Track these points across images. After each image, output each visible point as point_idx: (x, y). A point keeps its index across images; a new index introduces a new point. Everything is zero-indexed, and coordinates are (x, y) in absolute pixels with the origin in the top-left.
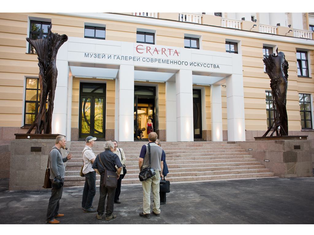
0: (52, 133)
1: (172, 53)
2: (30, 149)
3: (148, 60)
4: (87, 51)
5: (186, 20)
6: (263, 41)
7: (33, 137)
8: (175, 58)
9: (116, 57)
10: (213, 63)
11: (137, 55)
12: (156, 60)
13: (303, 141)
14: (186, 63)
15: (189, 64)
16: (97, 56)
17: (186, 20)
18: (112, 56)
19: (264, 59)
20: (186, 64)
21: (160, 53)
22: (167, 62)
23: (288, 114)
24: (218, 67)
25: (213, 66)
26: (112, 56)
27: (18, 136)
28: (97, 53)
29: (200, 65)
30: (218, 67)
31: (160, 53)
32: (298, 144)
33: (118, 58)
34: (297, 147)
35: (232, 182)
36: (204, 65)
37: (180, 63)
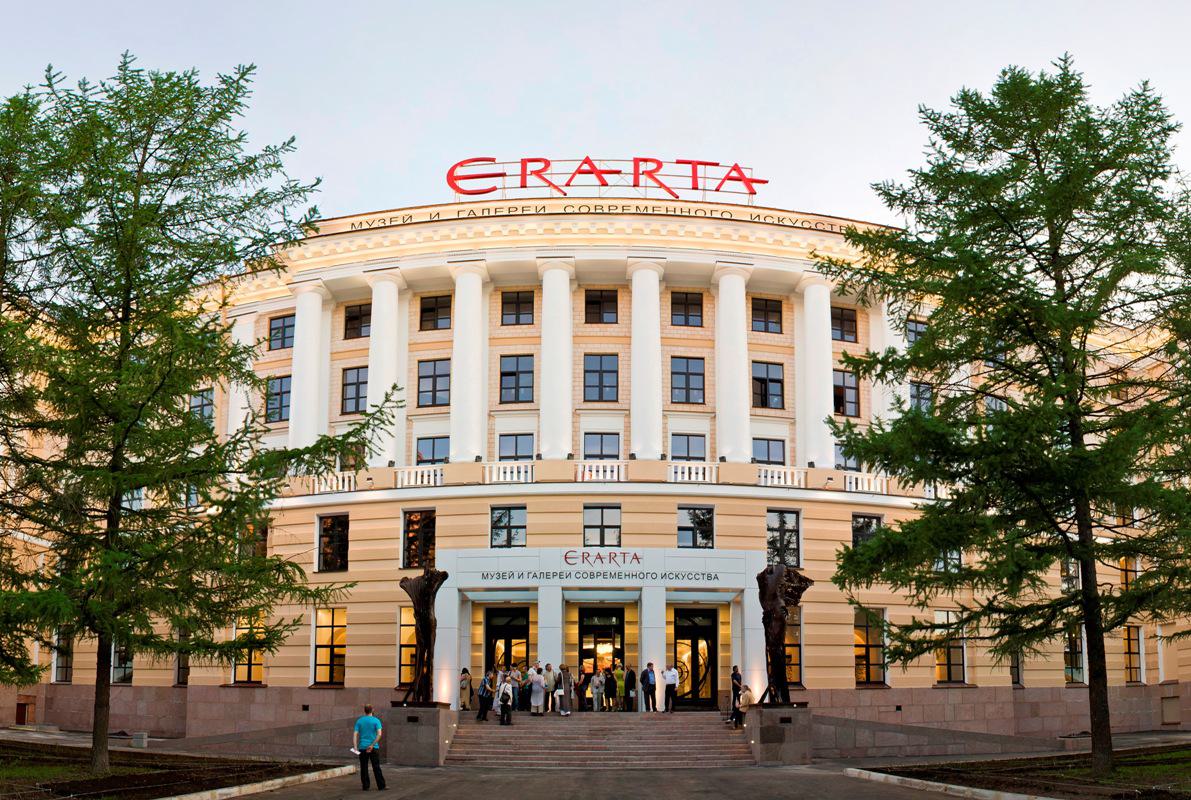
0: (434, 700)
1: (629, 559)
2: (406, 720)
3: (585, 575)
4: (486, 570)
5: (857, 488)
6: (677, 498)
7: (409, 705)
8: (634, 567)
9: (531, 575)
10: (707, 571)
11: (567, 568)
12: (599, 574)
13: (799, 709)
14: (654, 575)
15: (659, 577)
16: (501, 576)
17: (857, 488)
18: (526, 574)
19: (842, 549)
20: (654, 576)
21: (606, 561)
22: (619, 576)
23: (1108, 677)
24: (716, 577)
25: (706, 577)
26: (526, 574)
27: (395, 704)
28: (501, 571)
29: (680, 576)
30: (716, 577)
31: (606, 561)
32: (787, 716)
33: (535, 576)
34: (786, 720)
35: (961, 778)
36: (688, 576)
37: (644, 576)
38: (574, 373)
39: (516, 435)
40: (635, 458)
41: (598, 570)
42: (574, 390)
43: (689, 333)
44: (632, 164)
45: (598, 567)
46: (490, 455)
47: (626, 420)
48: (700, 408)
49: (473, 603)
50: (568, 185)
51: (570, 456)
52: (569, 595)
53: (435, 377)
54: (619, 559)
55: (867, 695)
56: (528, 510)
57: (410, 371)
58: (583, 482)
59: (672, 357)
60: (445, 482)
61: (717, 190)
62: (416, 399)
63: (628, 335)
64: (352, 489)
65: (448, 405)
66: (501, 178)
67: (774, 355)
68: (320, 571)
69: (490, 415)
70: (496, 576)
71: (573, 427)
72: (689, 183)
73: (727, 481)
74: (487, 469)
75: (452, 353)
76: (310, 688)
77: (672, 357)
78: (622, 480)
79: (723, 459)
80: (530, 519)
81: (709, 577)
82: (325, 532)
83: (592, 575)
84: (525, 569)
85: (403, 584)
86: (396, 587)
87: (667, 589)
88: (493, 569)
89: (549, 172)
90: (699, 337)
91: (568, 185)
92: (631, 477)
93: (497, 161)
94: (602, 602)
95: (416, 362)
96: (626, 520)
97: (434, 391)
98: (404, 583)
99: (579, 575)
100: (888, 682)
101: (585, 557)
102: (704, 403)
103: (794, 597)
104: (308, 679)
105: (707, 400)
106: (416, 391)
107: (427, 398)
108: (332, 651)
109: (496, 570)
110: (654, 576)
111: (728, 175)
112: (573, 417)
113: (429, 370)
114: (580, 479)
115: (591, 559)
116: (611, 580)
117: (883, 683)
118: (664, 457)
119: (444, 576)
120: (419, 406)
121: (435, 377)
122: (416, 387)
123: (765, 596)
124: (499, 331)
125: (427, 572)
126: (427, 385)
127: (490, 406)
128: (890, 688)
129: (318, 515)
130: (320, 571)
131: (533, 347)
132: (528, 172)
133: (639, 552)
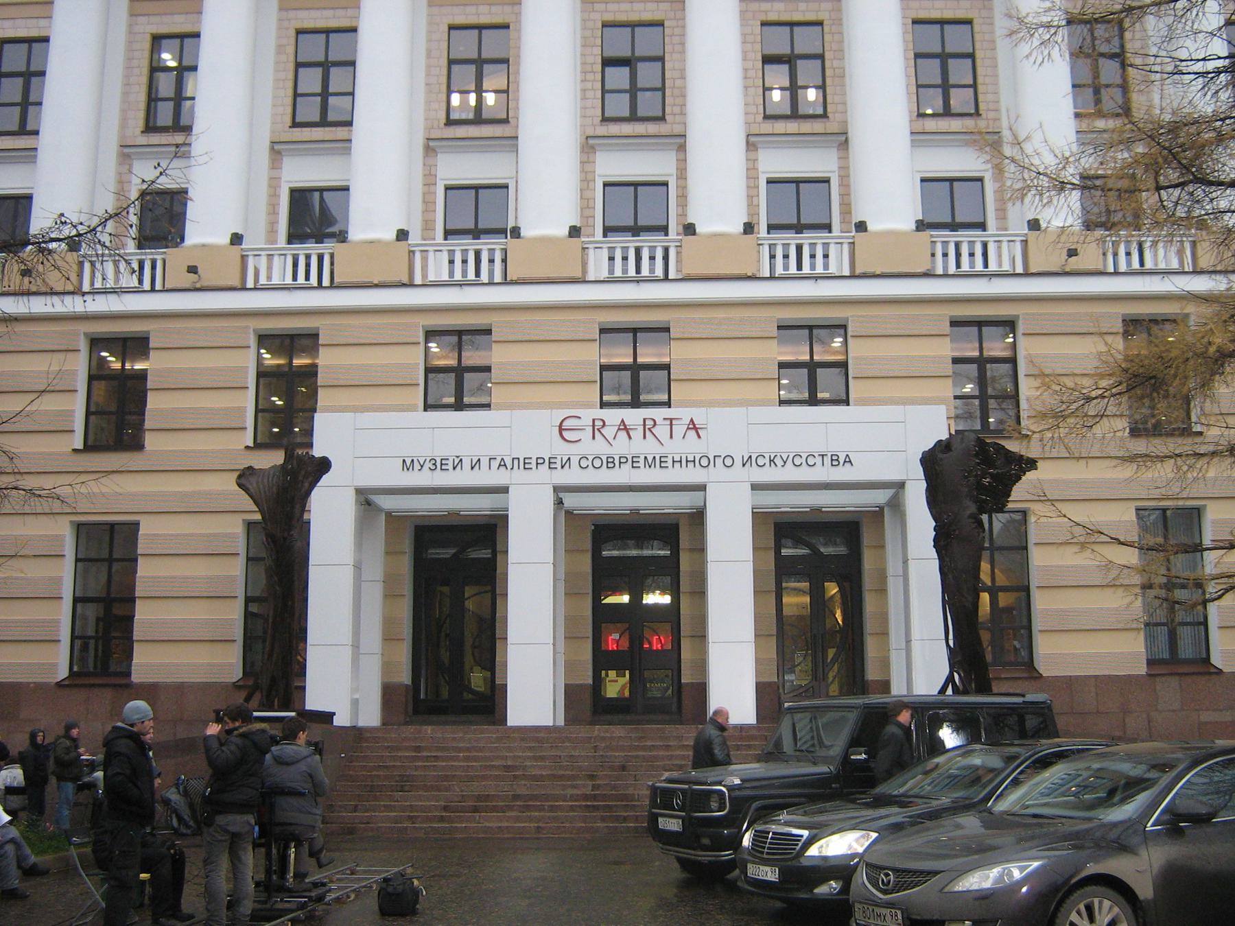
1: (679, 430)
4: (409, 452)
9: (495, 464)
11: (561, 449)
12: (623, 460)
14: (728, 461)
15: (738, 462)
16: (439, 464)
18: (484, 462)
20: (728, 462)
21: (637, 434)
22: (662, 462)
25: (827, 460)
26: (484, 462)
28: (439, 453)
29: (778, 461)
30: (848, 461)
31: (637, 434)
33: (502, 464)
36: (794, 459)
37: (707, 461)
38: (583, 64)
39: (636, 185)
40: (694, 233)
41: (624, 452)
42: (584, 98)
45: (622, 446)
46: (428, 226)
48: (818, 126)
49: (389, 515)
51: (575, 232)
52: (570, 501)
53: (326, 66)
55: (1169, 691)
56: (495, 337)
57: (280, 49)
58: (255, 289)
59: (764, 24)
60: (687, 270)
62: (289, 110)
64: (158, 286)
65: (349, 124)
67: (330, 13)
68: (89, 447)
69: (272, 149)
70: (428, 465)
71: (583, 171)
73: (870, 270)
74: (418, 256)
75: (358, 18)
76: (59, 685)
77: (764, 24)
80: (498, 356)
81: (835, 461)
82: (954, 326)
83: (610, 463)
84: (484, 451)
85: (243, 481)
86: (228, 484)
87: (755, 487)
88: (422, 449)
92: (168, 286)
94: (635, 512)
95: (293, 33)
96: (677, 353)
97: (325, 94)
98: (245, 477)
100: (1216, 660)
101: (597, 428)
104: (55, 665)
106: (290, 92)
107: (310, 111)
108: (108, 610)
109: (429, 453)
110: (728, 462)
112: (582, 151)
113: (314, 49)
115: (609, 432)
117: (1207, 660)
118: (749, 228)
119: (324, 465)
120: (295, 124)
121: (326, 66)
122: (290, 84)
125: (289, 457)
126: (311, 80)
127: (428, 129)
128: (1220, 672)
129: (86, 334)
130: (89, 447)
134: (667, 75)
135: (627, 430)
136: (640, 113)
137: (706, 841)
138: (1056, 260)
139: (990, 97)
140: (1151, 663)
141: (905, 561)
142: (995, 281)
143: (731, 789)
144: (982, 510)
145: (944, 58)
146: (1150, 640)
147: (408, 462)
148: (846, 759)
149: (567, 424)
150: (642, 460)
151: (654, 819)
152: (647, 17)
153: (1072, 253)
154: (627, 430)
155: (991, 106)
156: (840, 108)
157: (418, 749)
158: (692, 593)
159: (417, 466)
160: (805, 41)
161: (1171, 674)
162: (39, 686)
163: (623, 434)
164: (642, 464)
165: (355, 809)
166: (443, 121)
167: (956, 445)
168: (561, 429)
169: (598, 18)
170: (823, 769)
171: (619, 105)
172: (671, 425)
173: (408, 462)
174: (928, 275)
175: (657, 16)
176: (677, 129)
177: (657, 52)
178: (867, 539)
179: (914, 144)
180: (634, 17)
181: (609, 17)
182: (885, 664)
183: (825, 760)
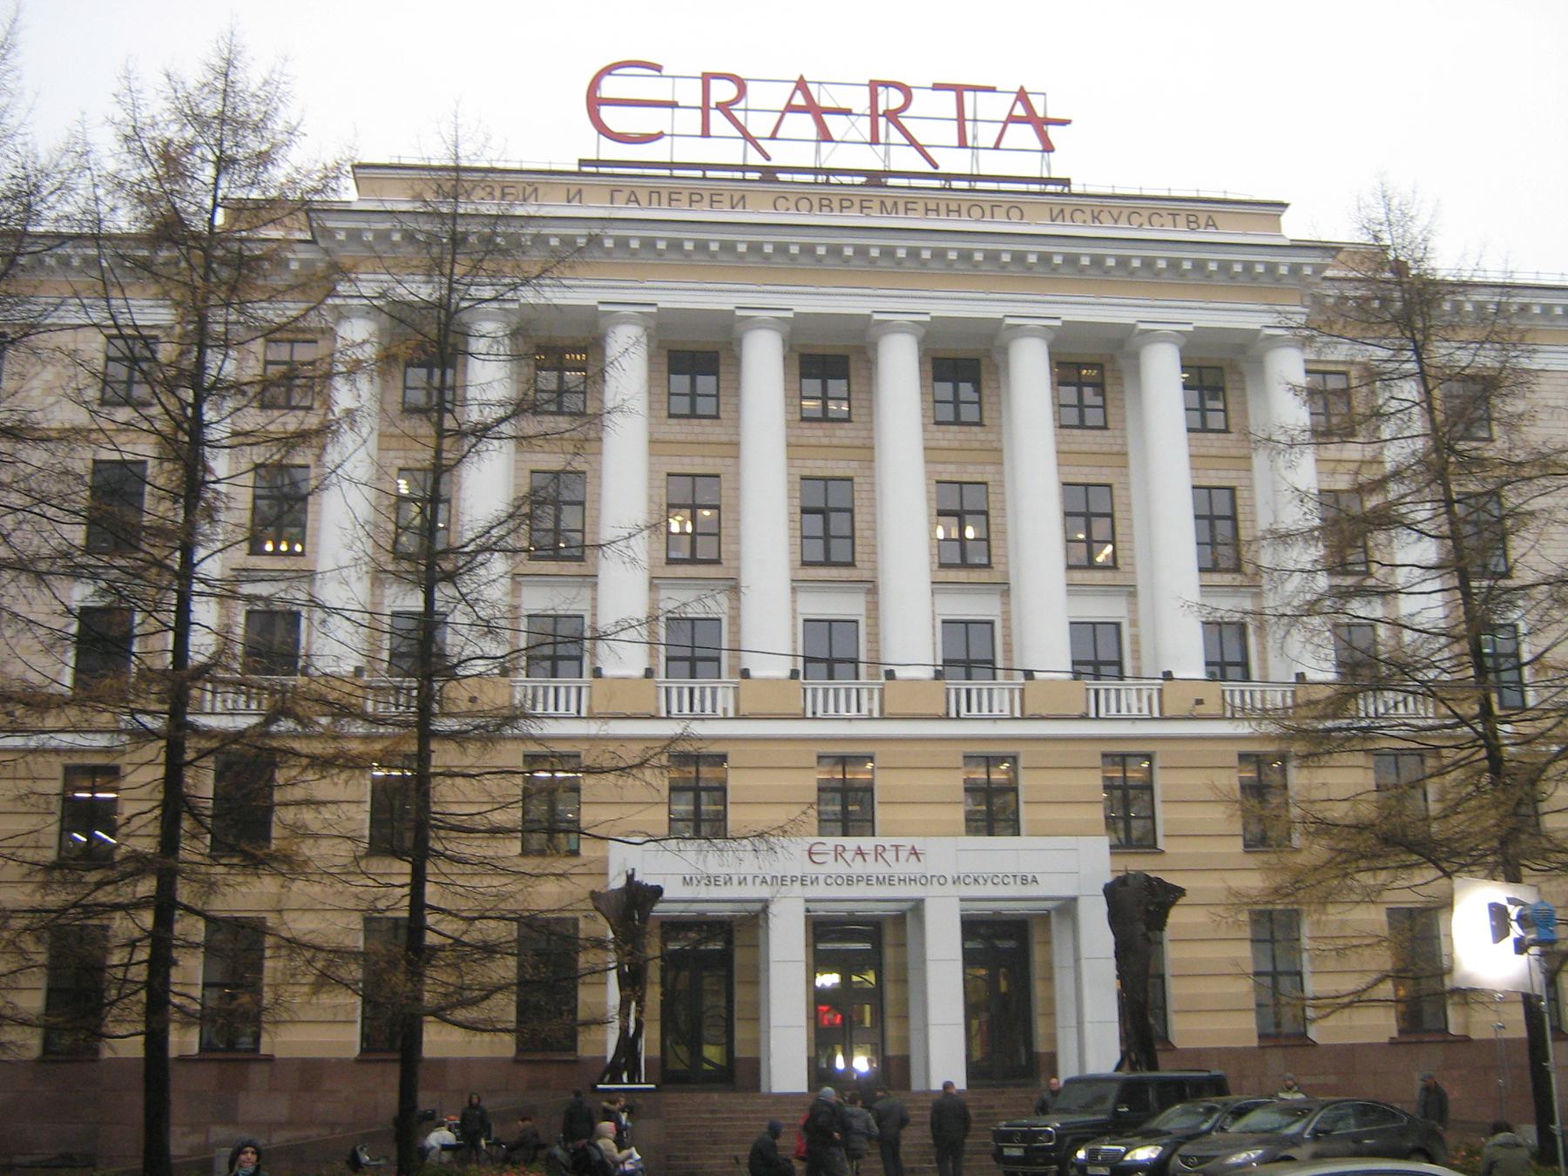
1: (903, 855)
9: (758, 881)
11: (811, 869)
14: (942, 880)
15: (950, 881)
18: (749, 879)
20: (942, 881)
21: (871, 858)
22: (888, 880)
26: (749, 879)
30: (1035, 880)
31: (871, 858)
33: (764, 881)
37: (925, 880)
43: (962, 436)
44: (867, 89)
45: (858, 867)
47: (870, 598)
50: (773, 137)
52: (812, 906)
54: (890, 856)
61: (997, 147)
63: (867, 442)
66: (669, 110)
72: (950, 133)
78: (818, 716)
79: (1029, 674)
81: (1024, 881)
83: (850, 881)
87: (962, 900)
89: (741, 105)
90: (976, 445)
91: (773, 137)
92: (1028, 712)
93: (664, 73)
99: (831, 880)
101: (839, 853)
102: (988, 566)
103: (1157, 920)
105: (994, 559)
111: (1010, 115)
114: (953, 714)
115: (848, 856)
116: (880, 887)
123: (1116, 918)
124: (664, 428)
127: (652, 567)
131: (719, 461)
132: (713, 105)
133: (918, 843)
134: (857, 525)
135: (862, 854)
136: (834, 559)
137: (1040, 1161)
138: (1186, 706)
139: (1127, 553)
140: (1261, 1036)
141: (1077, 960)
142: (1138, 724)
143: (1055, 1129)
144: (1149, 929)
145: (1088, 516)
146: (1260, 1017)
147: (688, 878)
148: (1115, 1113)
149: (815, 849)
150: (874, 879)
151: (1000, 1150)
152: (839, 473)
153: (1199, 702)
154: (862, 854)
155: (1128, 560)
156: (1003, 560)
157: (712, 1112)
158: (897, 981)
159: (695, 881)
160: (972, 500)
161: (1275, 1046)
162: (340, 1062)
163: (859, 858)
164: (874, 882)
165: (687, 1158)
166: (664, 560)
167: (1130, 882)
168: (810, 853)
169: (798, 472)
170: (1103, 1117)
171: (682, 405)
172: (897, 851)
173: (688, 878)
174: (1084, 717)
175: (849, 473)
176: (866, 575)
177: (848, 505)
178: (1036, 935)
179: (1069, 593)
180: (828, 473)
181: (807, 473)
182: (1052, 1038)
183: (1101, 1112)
